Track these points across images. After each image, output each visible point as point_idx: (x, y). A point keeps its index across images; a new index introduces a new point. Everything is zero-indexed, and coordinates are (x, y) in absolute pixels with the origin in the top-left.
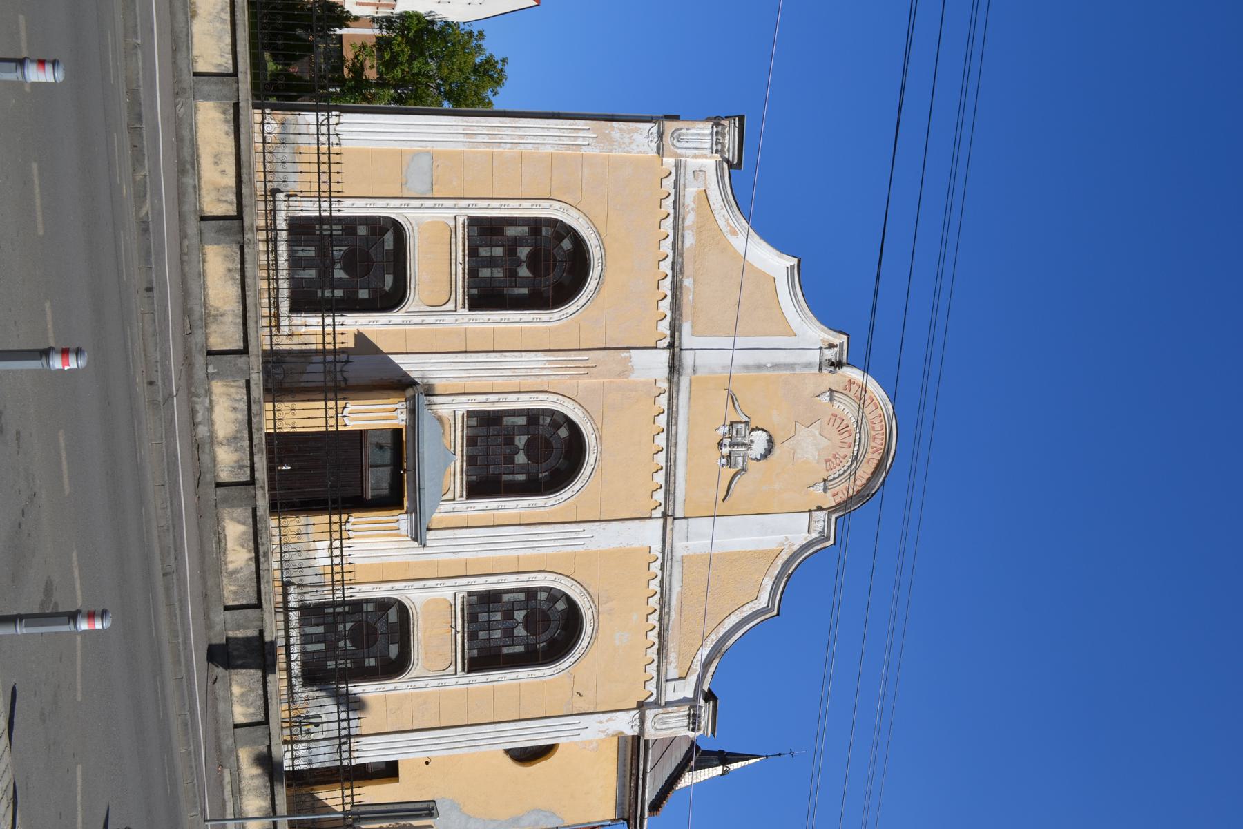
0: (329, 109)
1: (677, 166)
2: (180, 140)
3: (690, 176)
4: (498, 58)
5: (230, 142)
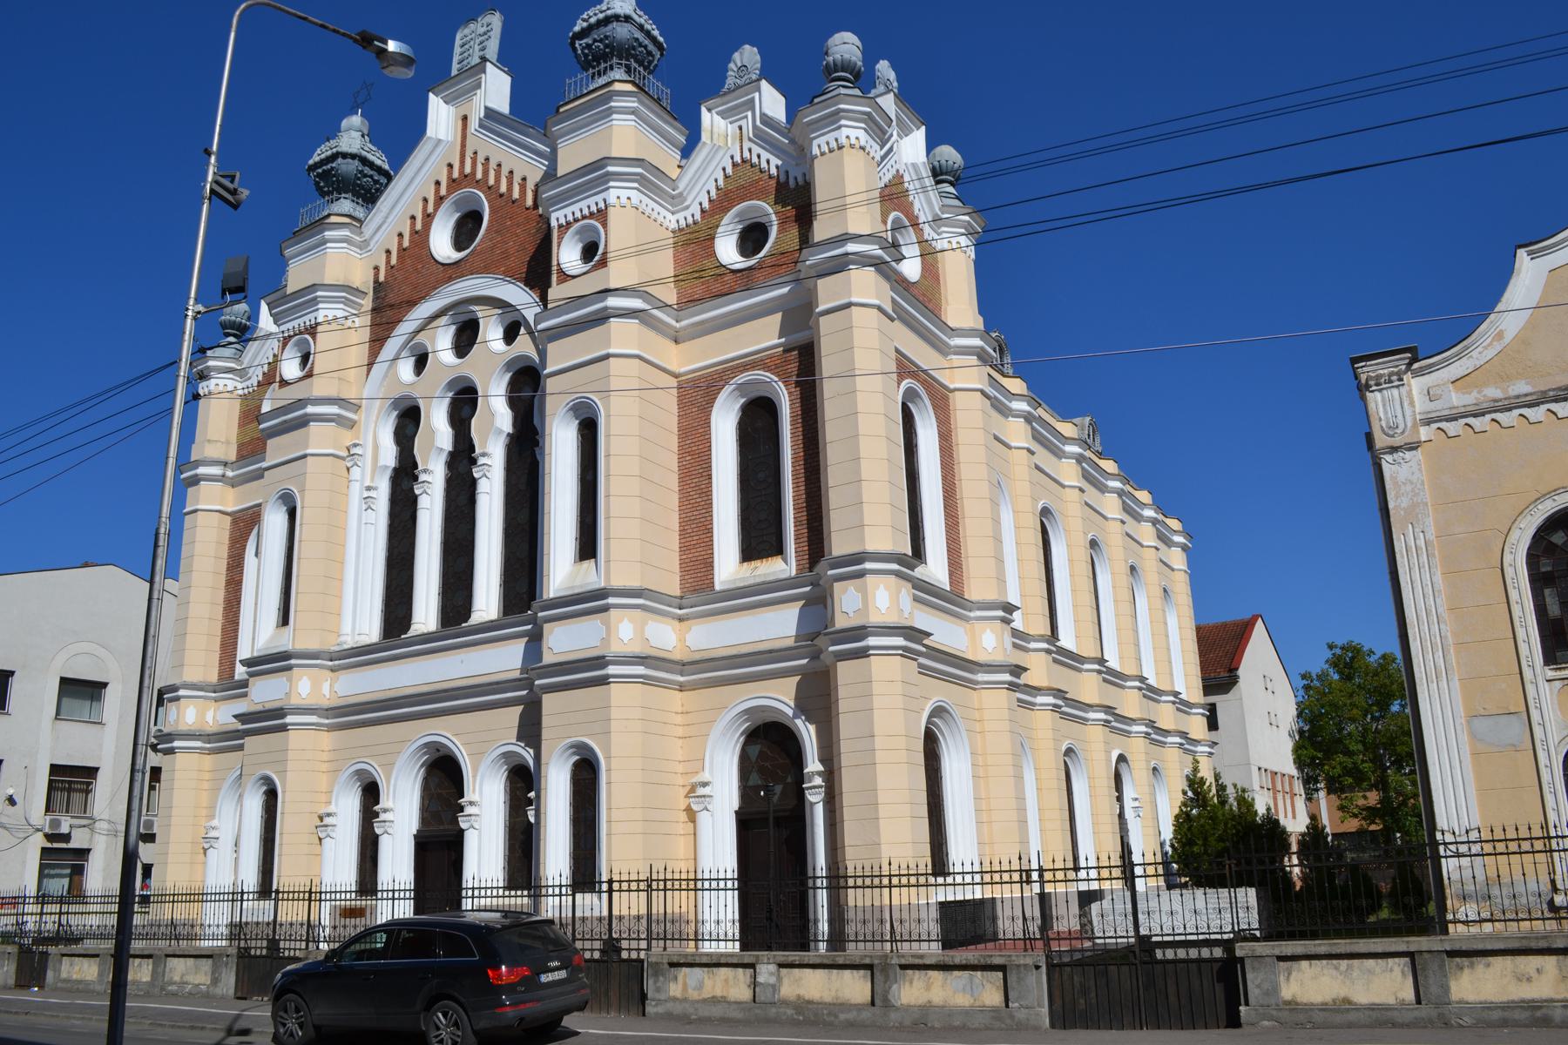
0: (1435, 844)
1: (1428, 422)
2: (1504, 1023)
3: (1437, 405)
4: (1328, 654)
5: (1498, 962)
